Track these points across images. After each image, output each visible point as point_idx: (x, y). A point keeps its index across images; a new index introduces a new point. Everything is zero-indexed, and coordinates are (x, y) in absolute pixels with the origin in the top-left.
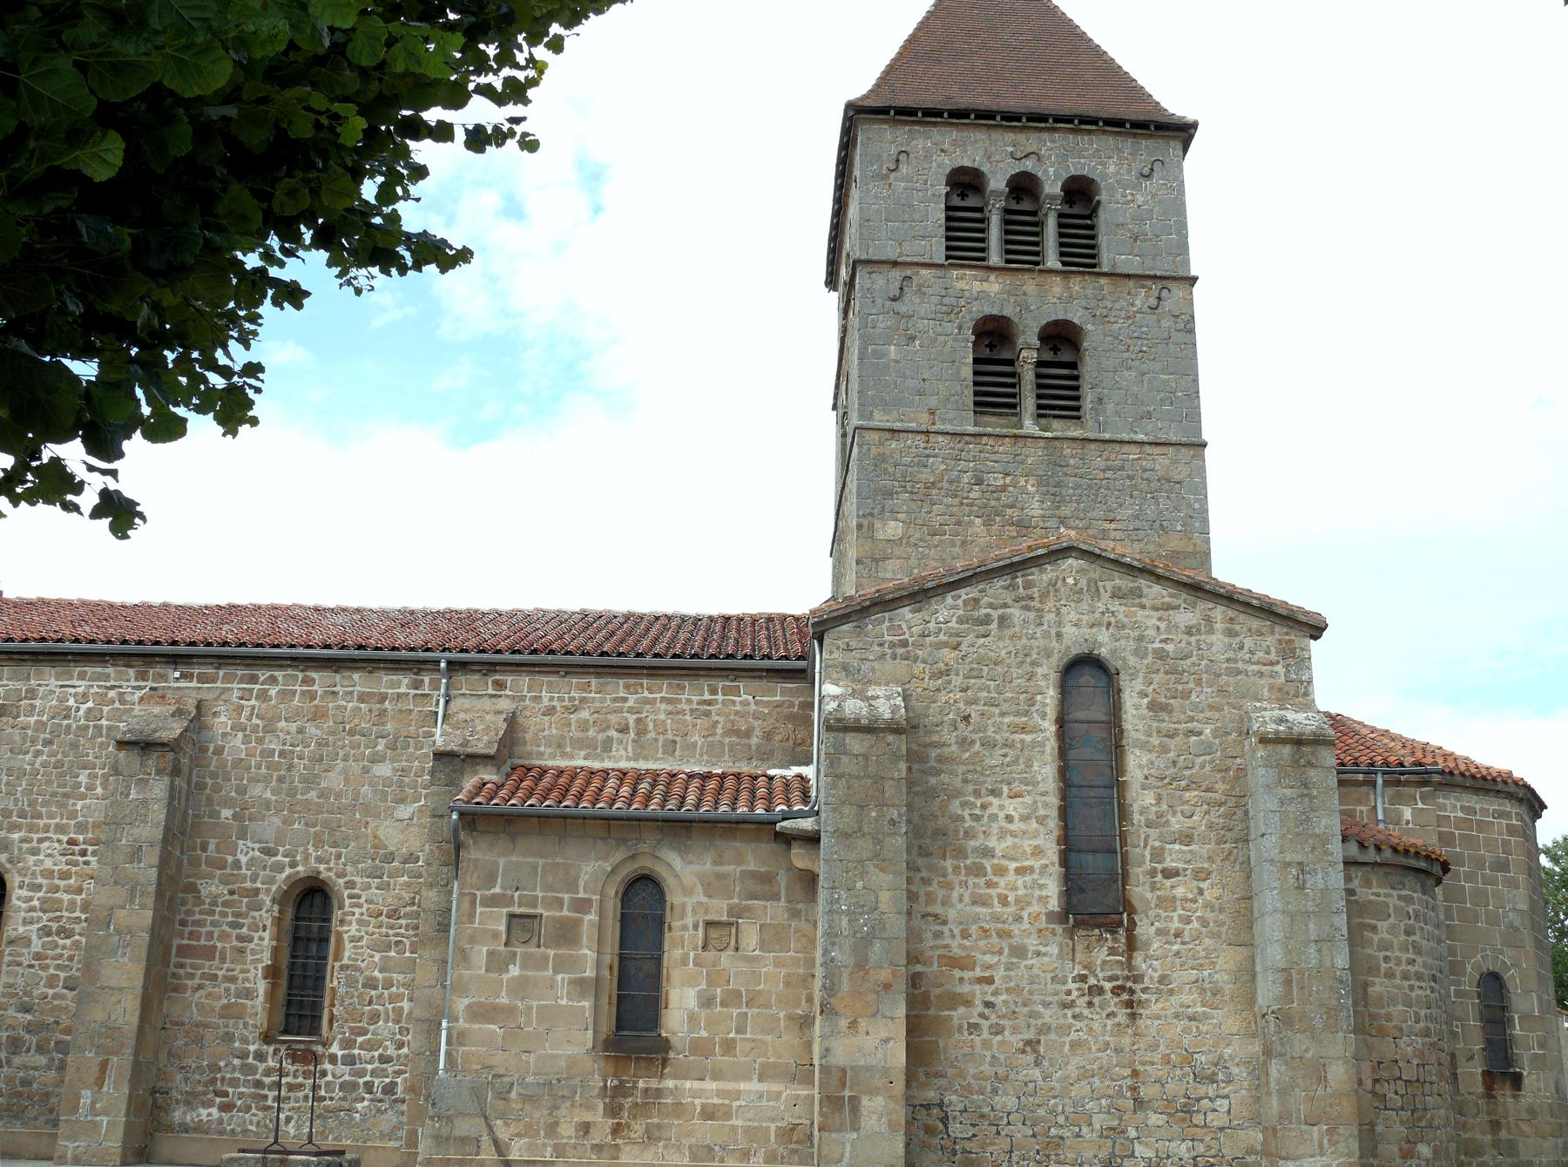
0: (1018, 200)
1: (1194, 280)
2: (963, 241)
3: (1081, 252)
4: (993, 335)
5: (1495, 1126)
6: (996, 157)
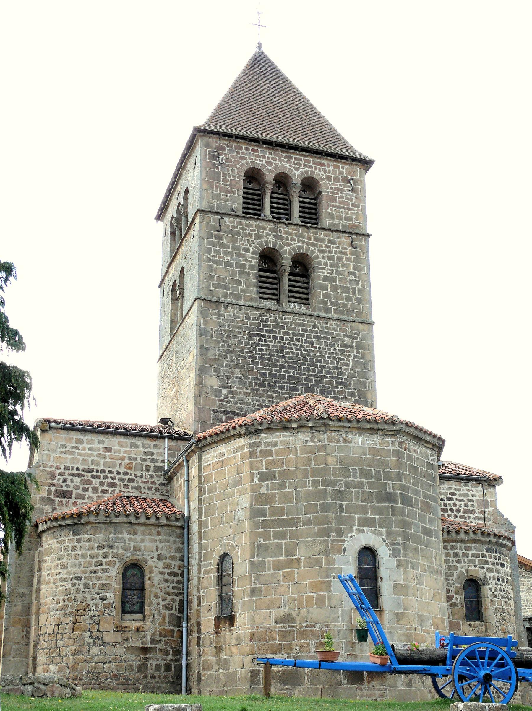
0: (279, 187)
1: (369, 236)
2: (252, 207)
3: (311, 216)
4: (268, 258)
5: (218, 650)
6: (271, 164)
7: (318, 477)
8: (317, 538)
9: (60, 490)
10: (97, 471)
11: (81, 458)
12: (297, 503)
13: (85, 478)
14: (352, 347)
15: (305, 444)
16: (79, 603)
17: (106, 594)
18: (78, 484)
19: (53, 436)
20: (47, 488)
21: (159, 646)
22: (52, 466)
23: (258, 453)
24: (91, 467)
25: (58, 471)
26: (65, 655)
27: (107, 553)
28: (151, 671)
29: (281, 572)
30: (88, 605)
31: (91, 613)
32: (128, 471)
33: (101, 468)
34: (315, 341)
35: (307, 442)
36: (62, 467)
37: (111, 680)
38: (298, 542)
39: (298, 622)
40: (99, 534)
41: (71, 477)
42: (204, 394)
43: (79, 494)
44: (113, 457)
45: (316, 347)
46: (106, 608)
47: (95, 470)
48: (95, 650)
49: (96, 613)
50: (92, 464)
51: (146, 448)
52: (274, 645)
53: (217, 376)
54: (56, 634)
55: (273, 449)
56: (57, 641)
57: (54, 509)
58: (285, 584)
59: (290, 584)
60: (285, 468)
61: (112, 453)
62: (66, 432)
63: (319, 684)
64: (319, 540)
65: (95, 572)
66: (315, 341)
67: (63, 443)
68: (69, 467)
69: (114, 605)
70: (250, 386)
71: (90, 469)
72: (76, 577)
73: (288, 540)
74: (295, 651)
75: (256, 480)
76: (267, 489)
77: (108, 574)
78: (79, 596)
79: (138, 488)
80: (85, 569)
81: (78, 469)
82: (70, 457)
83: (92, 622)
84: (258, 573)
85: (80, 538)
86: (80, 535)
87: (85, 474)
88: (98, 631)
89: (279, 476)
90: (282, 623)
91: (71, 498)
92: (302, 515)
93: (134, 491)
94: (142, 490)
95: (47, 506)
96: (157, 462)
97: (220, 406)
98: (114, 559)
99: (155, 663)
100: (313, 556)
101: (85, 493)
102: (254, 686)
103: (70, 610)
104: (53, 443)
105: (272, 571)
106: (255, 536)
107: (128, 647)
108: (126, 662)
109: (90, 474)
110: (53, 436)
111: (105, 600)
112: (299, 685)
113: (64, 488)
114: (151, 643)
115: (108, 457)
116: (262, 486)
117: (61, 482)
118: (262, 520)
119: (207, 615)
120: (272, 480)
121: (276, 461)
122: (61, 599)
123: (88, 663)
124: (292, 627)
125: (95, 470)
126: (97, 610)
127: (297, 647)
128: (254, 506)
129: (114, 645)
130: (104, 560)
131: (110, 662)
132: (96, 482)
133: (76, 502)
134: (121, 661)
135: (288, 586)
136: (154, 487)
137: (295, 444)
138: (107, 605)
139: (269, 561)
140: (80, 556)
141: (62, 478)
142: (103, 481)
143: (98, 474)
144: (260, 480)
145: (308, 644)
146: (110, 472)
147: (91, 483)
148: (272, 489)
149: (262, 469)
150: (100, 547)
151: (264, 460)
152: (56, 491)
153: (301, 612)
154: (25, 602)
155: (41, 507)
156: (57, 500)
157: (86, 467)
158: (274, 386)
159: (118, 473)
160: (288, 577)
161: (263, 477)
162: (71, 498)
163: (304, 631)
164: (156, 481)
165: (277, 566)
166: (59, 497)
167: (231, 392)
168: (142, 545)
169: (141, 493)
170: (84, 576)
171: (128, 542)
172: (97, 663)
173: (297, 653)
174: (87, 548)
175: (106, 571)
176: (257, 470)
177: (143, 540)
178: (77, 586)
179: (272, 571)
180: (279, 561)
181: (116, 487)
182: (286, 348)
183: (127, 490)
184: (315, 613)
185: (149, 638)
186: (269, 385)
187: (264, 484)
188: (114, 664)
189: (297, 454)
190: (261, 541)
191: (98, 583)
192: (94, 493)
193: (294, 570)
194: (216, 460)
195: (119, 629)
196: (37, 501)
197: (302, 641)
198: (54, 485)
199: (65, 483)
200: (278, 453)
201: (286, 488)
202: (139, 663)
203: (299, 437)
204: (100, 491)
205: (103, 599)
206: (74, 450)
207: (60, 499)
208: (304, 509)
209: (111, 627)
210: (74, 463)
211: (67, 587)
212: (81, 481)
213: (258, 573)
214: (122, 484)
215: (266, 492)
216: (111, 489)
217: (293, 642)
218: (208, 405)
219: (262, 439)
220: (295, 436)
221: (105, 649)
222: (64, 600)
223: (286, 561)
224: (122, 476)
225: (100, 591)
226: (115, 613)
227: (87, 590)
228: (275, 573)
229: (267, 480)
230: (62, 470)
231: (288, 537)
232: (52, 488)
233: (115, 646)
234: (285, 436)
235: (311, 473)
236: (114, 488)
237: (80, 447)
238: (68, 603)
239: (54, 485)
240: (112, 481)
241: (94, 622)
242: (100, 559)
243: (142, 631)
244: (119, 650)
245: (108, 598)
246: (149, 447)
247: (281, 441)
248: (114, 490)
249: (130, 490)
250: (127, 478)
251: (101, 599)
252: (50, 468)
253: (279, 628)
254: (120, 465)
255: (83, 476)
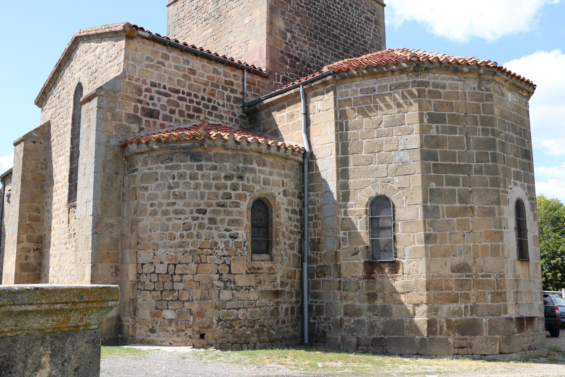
7: (487, 126)
8: (489, 188)
9: (147, 109)
10: (183, 93)
11: (167, 76)
12: (468, 149)
13: (172, 98)
14: (372, 21)
15: (472, 91)
16: (203, 240)
17: (238, 232)
18: (165, 104)
19: (138, 46)
20: (133, 104)
21: (287, 289)
22: (137, 80)
23: (427, 93)
24: (178, 88)
25: (144, 87)
26: (187, 299)
27: (237, 184)
28: (282, 316)
29: (455, 219)
30: (216, 243)
31: (220, 253)
32: (211, 97)
33: (186, 90)
34: (350, 8)
35: (474, 88)
36: (149, 83)
37: (245, 328)
38: (470, 189)
39: (474, 272)
40: (226, 162)
41: (158, 96)
42: (274, 34)
43: (166, 115)
44: (199, 81)
45: (350, 14)
46: (238, 247)
47: (181, 92)
48: (226, 295)
49: (225, 253)
50: (178, 84)
51: (227, 77)
52: (451, 294)
53: (283, 18)
54: (172, 276)
55: (442, 91)
56: (173, 282)
57: (141, 129)
58: (460, 233)
59: (465, 232)
60: (454, 113)
61: (197, 76)
62: (152, 43)
63: (498, 334)
64: (492, 190)
65: (223, 206)
66: (350, 8)
67: (149, 55)
68: (156, 83)
69: (246, 244)
70: (307, 35)
71: (177, 90)
72: (198, 210)
73: (461, 187)
74: (472, 301)
75: (425, 120)
76: (438, 132)
77: (239, 209)
78: (204, 232)
79: (221, 117)
80: (210, 201)
81: (164, 88)
82: (156, 73)
83: (221, 262)
84: (432, 219)
85: (202, 166)
86: (201, 161)
87: (172, 94)
88: (230, 272)
89: (448, 120)
90: (458, 272)
91: (158, 118)
92: (474, 162)
93: (217, 119)
94: (224, 120)
95: (134, 125)
96: (237, 93)
97: (286, 48)
98: (245, 192)
99: (285, 306)
100: (486, 206)
101: (172, 115)
102: (431, 337)
103: (191, 248)
104: (139, 53)
105: (446, 218)
106: (426, 180)
107: (262, 291)
108: (260, 307)
109: (176, 95)
110: (138, 46)
111: (236, 238)
112: (477, 334)
113: (151, 107)
114: (281, 286)
115: (193, 80)
116: (432, 128)
117: (147, 99)
118: (433, 164)
119: (351, 258)
120: (442, 123)
121: (445, 104)
122: (178, 234)
123: (219, 310)
124: (468, 276)
125: (181, 92)
126: (227, 250)
127: (474, 297)
128: (424, 148)
129: (248, 289)
130: (233, 193)
131: (244, 308)
132: (183, 104)
133: (163, 124)
134: (256, 307)
135: (463, 234)
136: (234, 118)
137: (464, 89)
138: (238, 245)
139: (443, 208)
140: (202, 186)
141: (148, 95)
142: (189, 104)
143: (185, 96)
144: (430, 121)
145: (485, 294)
146: (196, 96)
147: (178, 105)
148: (443, 132)
149: (431, 110)
150: (228, 177)
151: (433, 101)
152: (143, 109)
153: (477, 261)
154: (113, 234)
155: (128, 124)
156: (144, 119)
157: (173, 87)
158: (323, 41)
159: (203, 99)
160: (463, 225)
161: (433, 119)
162: (158, 118)
163: (480, 280)
164: (236, 113)
165: (452, 213)
166: (145, 116)
167: (293, 37)
168: (271, 178)
169: (223, 122)
170: (209, 209)
171: (258, 174)
172: (230, 309)
173: (475, 303)
174: (211, 177)
175: (237, 205)
176: (426, 110)
177: (271, 174)
178: (200, 221)
179: (446, 218)
180: (453, 208)
181: (201, 113)
182: (330, 8)
183: (211, 118)
184: (490, 263)
185: (278, 281)
186: (320, 38)
187: (434, 125)
188: (248, 309)
189: (466, 100)
190: (433, 185)
191: (227, 218)
192: (180, 116)
193: (468, 218)
194: (360, 95)
195: (253, 271)
196: (124, 117)
197: (479, 291)
198: (140, 102)
199: (152, 102)
200: (447, 96)
201: (456, 134)
202: (272, 308)
203: (467, 82)
204: (186, 115)
205: (233, 237)
206: (160, 66)
207: (147, 119)
208: (475, 157)
209: (243, 270)
210: (160, 80)
211: (186, 221)
212: (168, 101)
213: (432, 219)
214: (207, 110)
215: (436, 134)
216: (196, 114)
217: (470, 291)
218: (277, 45)
219: (429, 79)
220: (463, 81)
221: (237, 294)
222: (182, 236)
223: (460, 208)
224: (206, 102)
225: (230, 227)
226: (246, 251)
227: (214, 226)
228: (450, 220)
229: (437, 122)
230: (148, 86)
231: (461, 184)
232: (138, 104)
233: (249, 289)
234: (454, 80)
235: (480, 121)
236: (200, 114)
237: (166, 63)
238: (188, 240)
239: (140, 102)
240: (197, 106)
241: (224, 263)
242: (229, 190)
243: (273, 273)
244: (253, 295)
245: (240, 236)
246: (229, 76)
247: (450, 84)
248: (200, 116)
249: (213, 118)
250: (211, 104)
251: (231, 237)
252: (136, 81)
253: (455, 277)
254: (204, 90)
255: (170, 96)
